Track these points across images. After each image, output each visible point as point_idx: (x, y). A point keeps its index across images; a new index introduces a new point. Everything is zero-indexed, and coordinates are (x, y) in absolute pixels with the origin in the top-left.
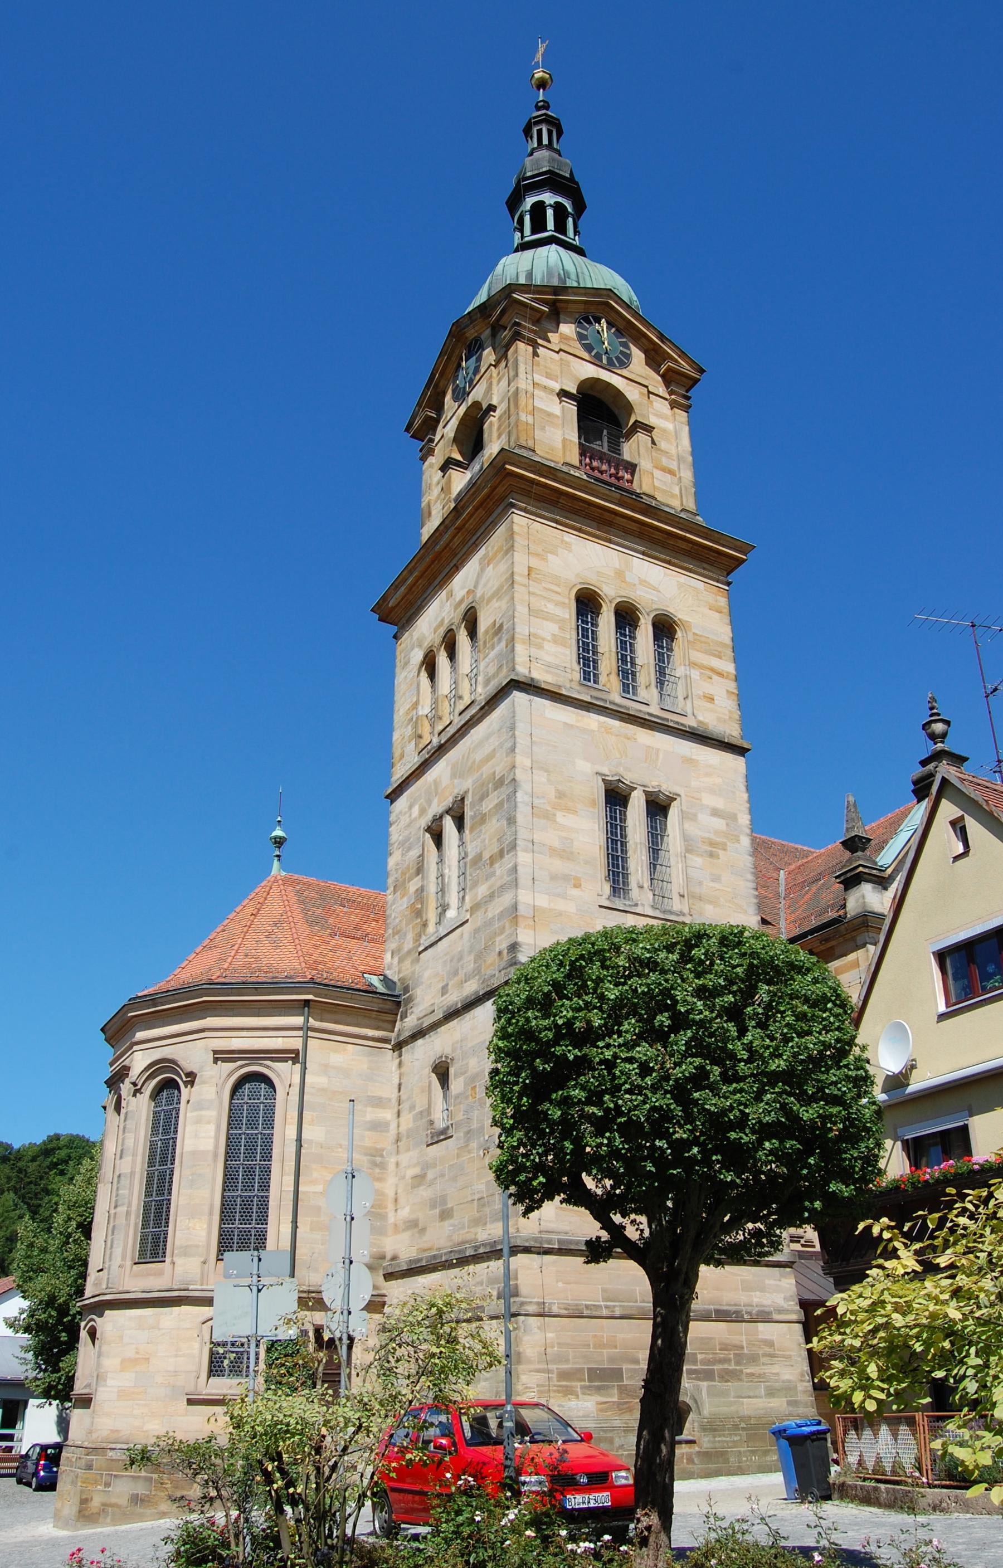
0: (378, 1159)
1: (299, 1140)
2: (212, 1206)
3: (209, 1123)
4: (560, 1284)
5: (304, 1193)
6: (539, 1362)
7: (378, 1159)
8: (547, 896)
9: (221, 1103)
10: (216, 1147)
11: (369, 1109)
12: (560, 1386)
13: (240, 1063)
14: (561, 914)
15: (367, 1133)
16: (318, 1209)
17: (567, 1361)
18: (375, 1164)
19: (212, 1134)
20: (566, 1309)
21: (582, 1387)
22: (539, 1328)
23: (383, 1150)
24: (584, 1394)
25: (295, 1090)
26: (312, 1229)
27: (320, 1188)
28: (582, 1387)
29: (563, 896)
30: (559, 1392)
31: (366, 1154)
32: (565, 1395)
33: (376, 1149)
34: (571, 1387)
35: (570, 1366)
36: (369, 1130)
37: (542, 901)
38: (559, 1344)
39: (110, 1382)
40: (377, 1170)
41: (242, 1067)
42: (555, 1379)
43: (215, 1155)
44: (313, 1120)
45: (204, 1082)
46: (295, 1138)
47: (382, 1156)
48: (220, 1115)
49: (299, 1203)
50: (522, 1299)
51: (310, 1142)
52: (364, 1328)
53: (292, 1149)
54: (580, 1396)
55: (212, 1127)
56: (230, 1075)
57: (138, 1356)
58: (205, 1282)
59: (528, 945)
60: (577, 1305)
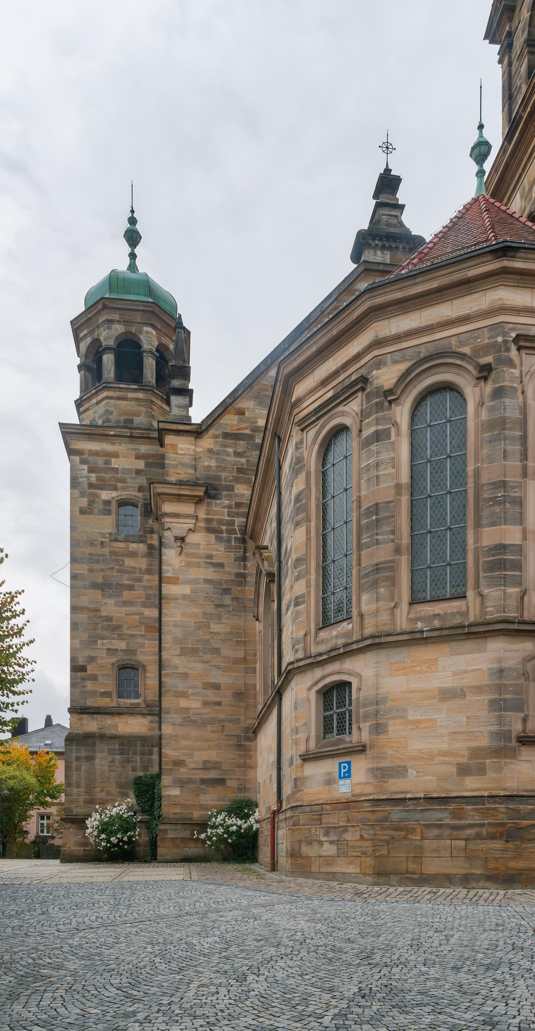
13: (321, 422)
41: (323, 427)
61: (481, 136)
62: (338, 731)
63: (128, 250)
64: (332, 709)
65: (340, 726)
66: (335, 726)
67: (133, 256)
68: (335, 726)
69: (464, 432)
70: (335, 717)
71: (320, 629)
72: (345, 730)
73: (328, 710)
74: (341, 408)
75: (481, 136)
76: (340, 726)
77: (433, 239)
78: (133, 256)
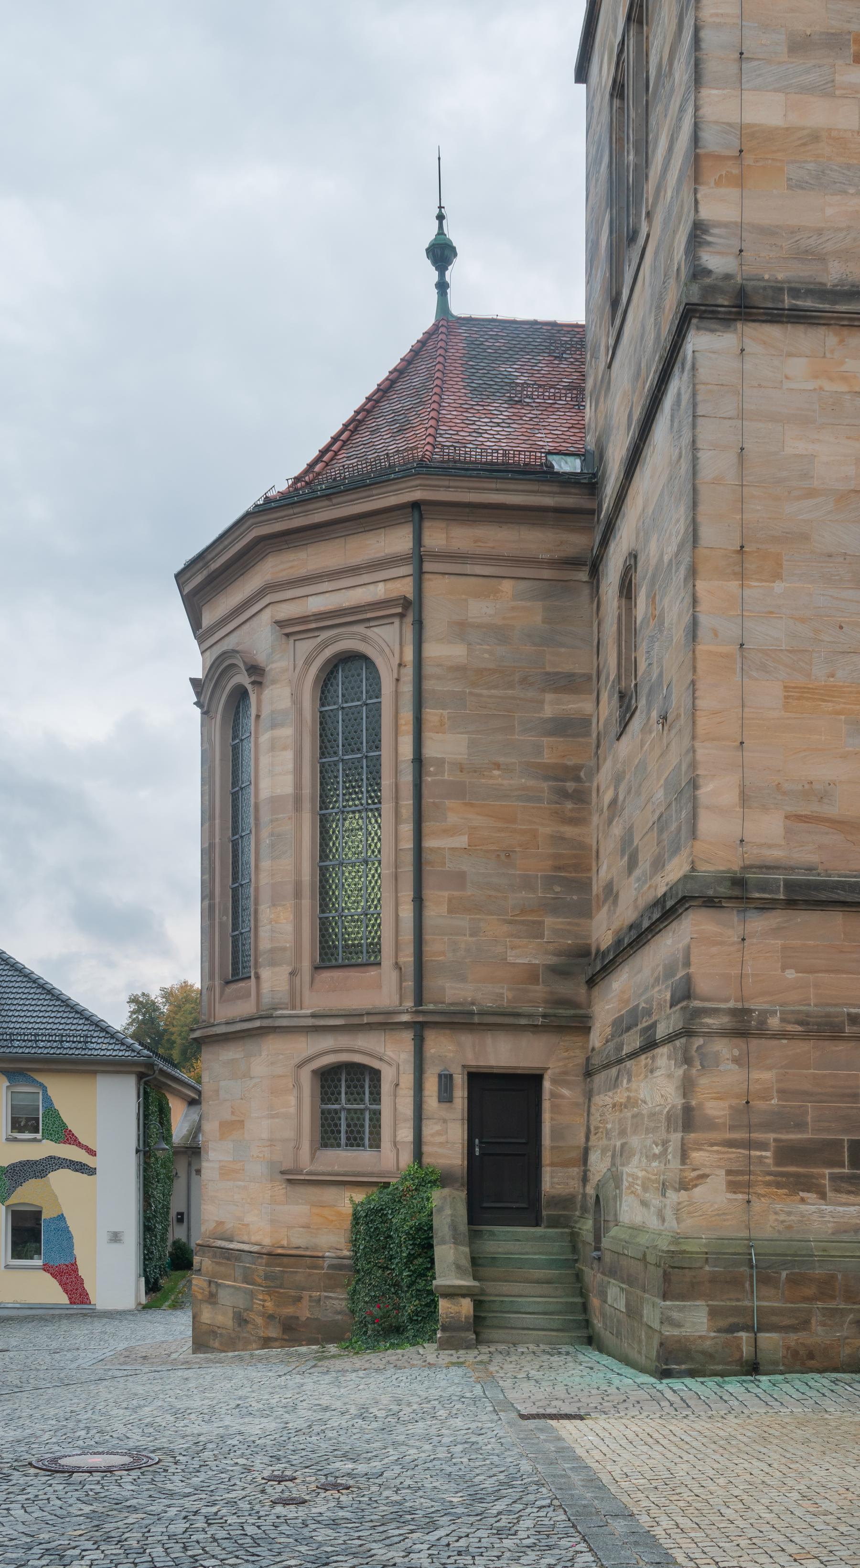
0: (570, 786)
1: (418, 760)
2: (298, 885)
3: (285, 748)
4: (791, 974)
5: (431, 850)
6: (732, 1128)
7: (570, 786)
8: (781, 97)
9: (300, 712)
10: (298, 785)
11: (549, 697)
12: (782, 1174)
13: (325, 635)
14: (815, 137)
15: (545, 740)
16: (460, 879)
17: (800, 1126)
18: (564, 794)
19: (290, 766)
20: (800, 1023)
21: (834, 1178)
22: (736, 1061)
23: (578, 768)
24: (837, 1190)
25: (408, 673)
26: (450, 911)
27: (462, 841)
28: (834, 1178)
29: (827, 90)
30: (779, 1185)
31: (546, 778)
32: (793, 1192)
33: (566, 768)
34: (810, 1176)
35: (805, 1136)
36: (550, 734)
37: (766, 110)
38: (782, 1092)
39: (212, 1155)
40: (569, 805)
41: (325, 645)
42: (770, 1161)
43: (298, 800)
44: (442, 724)
45: (274, 682)
46: (411, 757)
47: (578, 779)
48: (299, 733)
49: (426, 868)
50: (697, 1004)
51: (440, 762)
52: (179, 1041)
53: (407, 778)
54: (829, 1194)
55: (288, 756)
56: (308, 662)
57: (234, 1118)
58: (298, 1004)
59: (726, 225)
60: (828, 1015)
61: (442, 275)
62: (348, 1139)
63: (434, 275)
64: (337, 1101)
65: (352, 1132)
66: (343, 1128)
67: (442, 287)
68: (343, 1128)
69: (377, 742)
70: (343, 1115)
71: (228, 983)
72: (362, 1139)
73: (329, 1100)
74: (360, 629)
75: (442, 275)
76: (352, 1132)
77: (365, 404)
78: (442, 287)
